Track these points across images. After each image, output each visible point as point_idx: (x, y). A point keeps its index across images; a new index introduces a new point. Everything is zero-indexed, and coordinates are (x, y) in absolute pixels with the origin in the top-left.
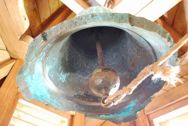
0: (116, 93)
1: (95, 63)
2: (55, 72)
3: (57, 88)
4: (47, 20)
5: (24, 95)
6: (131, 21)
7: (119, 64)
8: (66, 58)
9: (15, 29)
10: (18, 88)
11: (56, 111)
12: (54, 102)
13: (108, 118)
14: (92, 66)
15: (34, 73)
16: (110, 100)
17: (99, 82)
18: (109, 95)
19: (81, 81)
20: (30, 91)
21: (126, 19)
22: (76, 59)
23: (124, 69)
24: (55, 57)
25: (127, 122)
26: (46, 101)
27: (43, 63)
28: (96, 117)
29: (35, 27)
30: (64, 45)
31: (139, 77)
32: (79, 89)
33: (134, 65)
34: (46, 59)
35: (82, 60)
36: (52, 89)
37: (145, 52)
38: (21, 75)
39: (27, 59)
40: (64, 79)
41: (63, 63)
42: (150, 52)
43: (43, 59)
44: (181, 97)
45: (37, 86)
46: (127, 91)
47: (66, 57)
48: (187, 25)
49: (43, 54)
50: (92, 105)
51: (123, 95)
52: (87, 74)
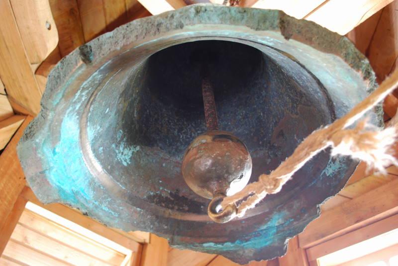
0: (243, 191)
1: (197, 129)
2: (107, 141)
3: (111, 176)
5: (34, 187)
6: (284, 28)
8: (134, 111)
9: (25, 48)
12: (102, 209)
14: (191, 135)
15: (60, 140)
16: (228, 206)
17: (206, 165)
19: (164, 165)
20: (49, 180)
21: (274, 21)
23: (261, 143)
24: (109, 107)
25: (262, 261)
27: (80, 119)
30: (131, 81)
31: (299, 152)
33: (283, 135)
35: (168, 121)
36: (98, 179)
38: (28, 143)
39: (45, 106)
40: (127, 158)
42: (322, 106)
43: (81, 108)
45: (66, 170)
46: (270, 184)
49: (82, 96)
50: (185, 219)
51: (260, 193)
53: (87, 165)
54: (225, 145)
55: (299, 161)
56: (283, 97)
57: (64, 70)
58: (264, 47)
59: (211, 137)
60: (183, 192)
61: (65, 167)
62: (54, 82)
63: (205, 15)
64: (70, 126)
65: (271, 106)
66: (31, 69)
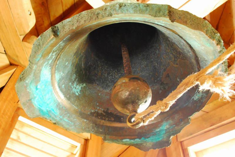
1: (119, 73)
4: (58, 18)
5: (25, 109)
6: (171, 15)
7: (150, 75)
10: (19, 103)
11: (66, 132)
12: (64, 121)
13: (133, 143)
14: (115, 77)
15: (40, 81)
17: (125, 95)
18: (138, 112)
19: (99, 94)
20: (33, 104)
22: (94, 66)
23: (156, 81)
24: (68, 61)
25: (157, 149)
26: (54, 119)
27: (52, 69)
28: (117, 141)
29: (43, 26)
31: (180, 88)
32: (97, 105)
33: (169, 76)
34: (56, 63)
36: (62, 103)
37: (185, 60)
40: (78, 91)
41: (77, 70)
42: (192, 60)
43: (52, 63)
44: (224, 120)
46: (163, 106)
47: (82, 62)
48: (234, 32)
51: (157, 111)
52: (107, 86)
53: (55, 95)
54: (136, 84)
55: (180, 93)
56: (169, 54)
57: (43, 40)
58: (159, 26)
59: (128, 79)
60: (111, 110)
61: (43, 96)
62: (37, 48)
63: (125, 8)
64: (46, 72)
65: (162, 59)
66: (19, 39)
